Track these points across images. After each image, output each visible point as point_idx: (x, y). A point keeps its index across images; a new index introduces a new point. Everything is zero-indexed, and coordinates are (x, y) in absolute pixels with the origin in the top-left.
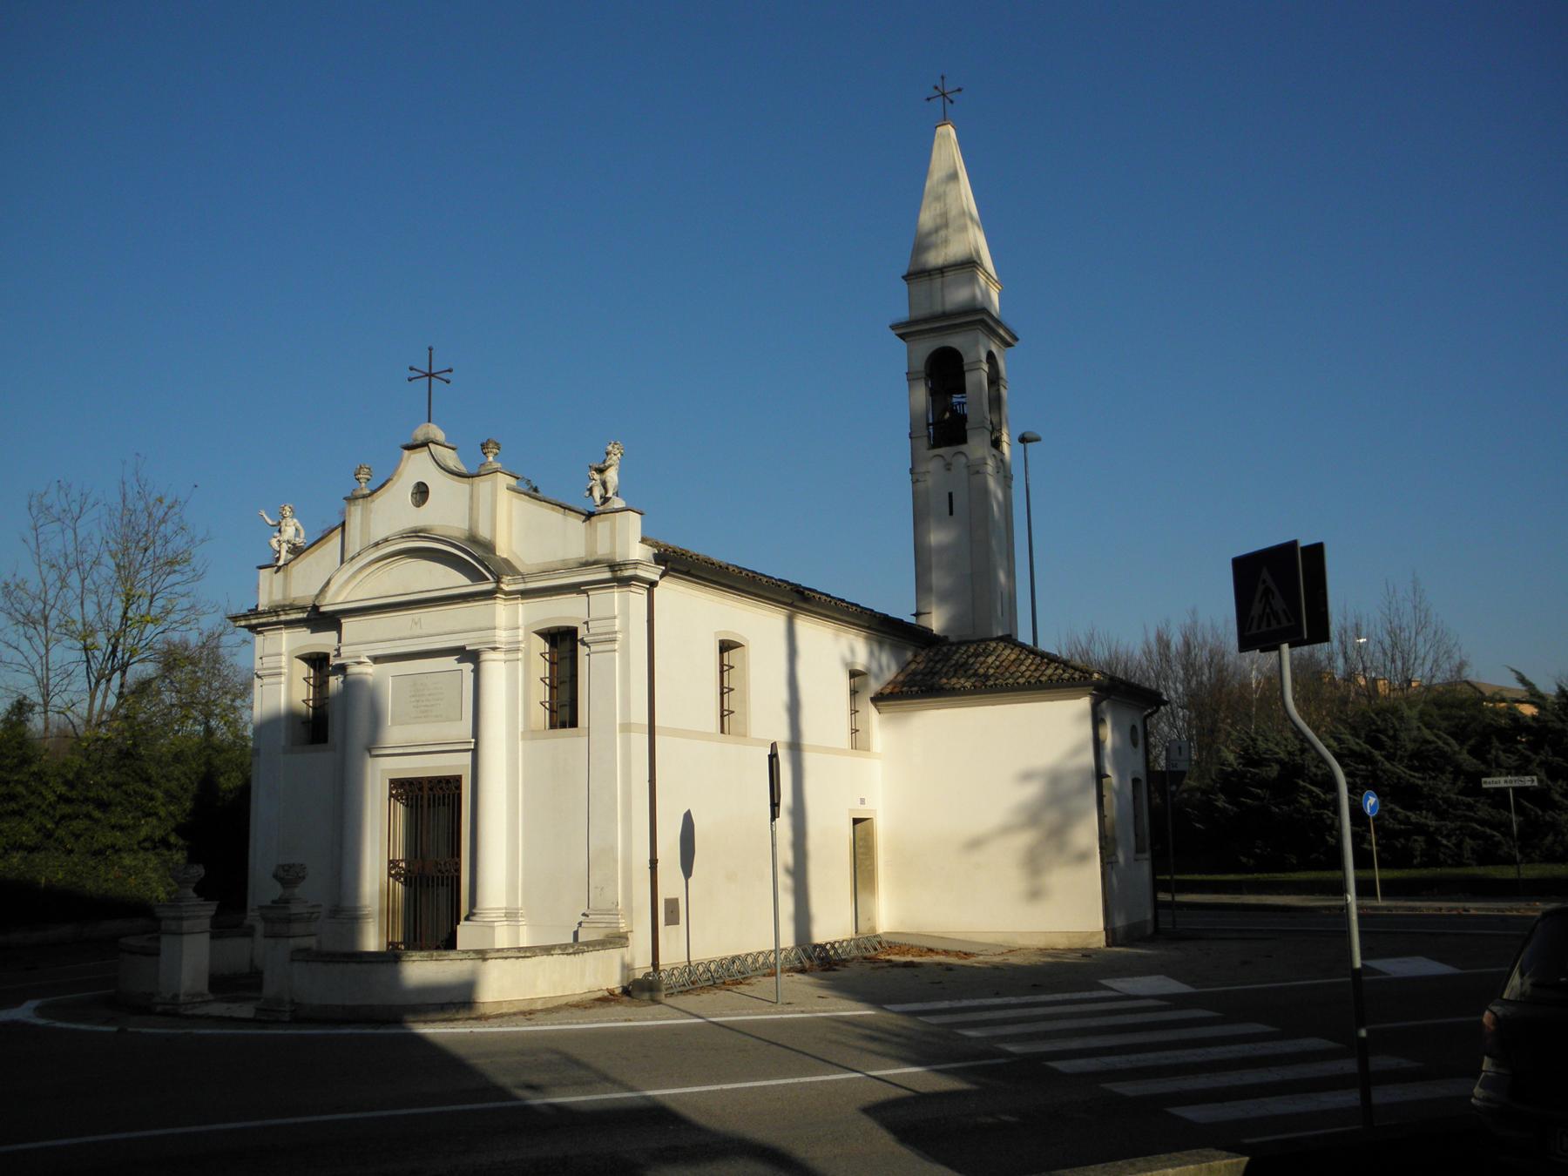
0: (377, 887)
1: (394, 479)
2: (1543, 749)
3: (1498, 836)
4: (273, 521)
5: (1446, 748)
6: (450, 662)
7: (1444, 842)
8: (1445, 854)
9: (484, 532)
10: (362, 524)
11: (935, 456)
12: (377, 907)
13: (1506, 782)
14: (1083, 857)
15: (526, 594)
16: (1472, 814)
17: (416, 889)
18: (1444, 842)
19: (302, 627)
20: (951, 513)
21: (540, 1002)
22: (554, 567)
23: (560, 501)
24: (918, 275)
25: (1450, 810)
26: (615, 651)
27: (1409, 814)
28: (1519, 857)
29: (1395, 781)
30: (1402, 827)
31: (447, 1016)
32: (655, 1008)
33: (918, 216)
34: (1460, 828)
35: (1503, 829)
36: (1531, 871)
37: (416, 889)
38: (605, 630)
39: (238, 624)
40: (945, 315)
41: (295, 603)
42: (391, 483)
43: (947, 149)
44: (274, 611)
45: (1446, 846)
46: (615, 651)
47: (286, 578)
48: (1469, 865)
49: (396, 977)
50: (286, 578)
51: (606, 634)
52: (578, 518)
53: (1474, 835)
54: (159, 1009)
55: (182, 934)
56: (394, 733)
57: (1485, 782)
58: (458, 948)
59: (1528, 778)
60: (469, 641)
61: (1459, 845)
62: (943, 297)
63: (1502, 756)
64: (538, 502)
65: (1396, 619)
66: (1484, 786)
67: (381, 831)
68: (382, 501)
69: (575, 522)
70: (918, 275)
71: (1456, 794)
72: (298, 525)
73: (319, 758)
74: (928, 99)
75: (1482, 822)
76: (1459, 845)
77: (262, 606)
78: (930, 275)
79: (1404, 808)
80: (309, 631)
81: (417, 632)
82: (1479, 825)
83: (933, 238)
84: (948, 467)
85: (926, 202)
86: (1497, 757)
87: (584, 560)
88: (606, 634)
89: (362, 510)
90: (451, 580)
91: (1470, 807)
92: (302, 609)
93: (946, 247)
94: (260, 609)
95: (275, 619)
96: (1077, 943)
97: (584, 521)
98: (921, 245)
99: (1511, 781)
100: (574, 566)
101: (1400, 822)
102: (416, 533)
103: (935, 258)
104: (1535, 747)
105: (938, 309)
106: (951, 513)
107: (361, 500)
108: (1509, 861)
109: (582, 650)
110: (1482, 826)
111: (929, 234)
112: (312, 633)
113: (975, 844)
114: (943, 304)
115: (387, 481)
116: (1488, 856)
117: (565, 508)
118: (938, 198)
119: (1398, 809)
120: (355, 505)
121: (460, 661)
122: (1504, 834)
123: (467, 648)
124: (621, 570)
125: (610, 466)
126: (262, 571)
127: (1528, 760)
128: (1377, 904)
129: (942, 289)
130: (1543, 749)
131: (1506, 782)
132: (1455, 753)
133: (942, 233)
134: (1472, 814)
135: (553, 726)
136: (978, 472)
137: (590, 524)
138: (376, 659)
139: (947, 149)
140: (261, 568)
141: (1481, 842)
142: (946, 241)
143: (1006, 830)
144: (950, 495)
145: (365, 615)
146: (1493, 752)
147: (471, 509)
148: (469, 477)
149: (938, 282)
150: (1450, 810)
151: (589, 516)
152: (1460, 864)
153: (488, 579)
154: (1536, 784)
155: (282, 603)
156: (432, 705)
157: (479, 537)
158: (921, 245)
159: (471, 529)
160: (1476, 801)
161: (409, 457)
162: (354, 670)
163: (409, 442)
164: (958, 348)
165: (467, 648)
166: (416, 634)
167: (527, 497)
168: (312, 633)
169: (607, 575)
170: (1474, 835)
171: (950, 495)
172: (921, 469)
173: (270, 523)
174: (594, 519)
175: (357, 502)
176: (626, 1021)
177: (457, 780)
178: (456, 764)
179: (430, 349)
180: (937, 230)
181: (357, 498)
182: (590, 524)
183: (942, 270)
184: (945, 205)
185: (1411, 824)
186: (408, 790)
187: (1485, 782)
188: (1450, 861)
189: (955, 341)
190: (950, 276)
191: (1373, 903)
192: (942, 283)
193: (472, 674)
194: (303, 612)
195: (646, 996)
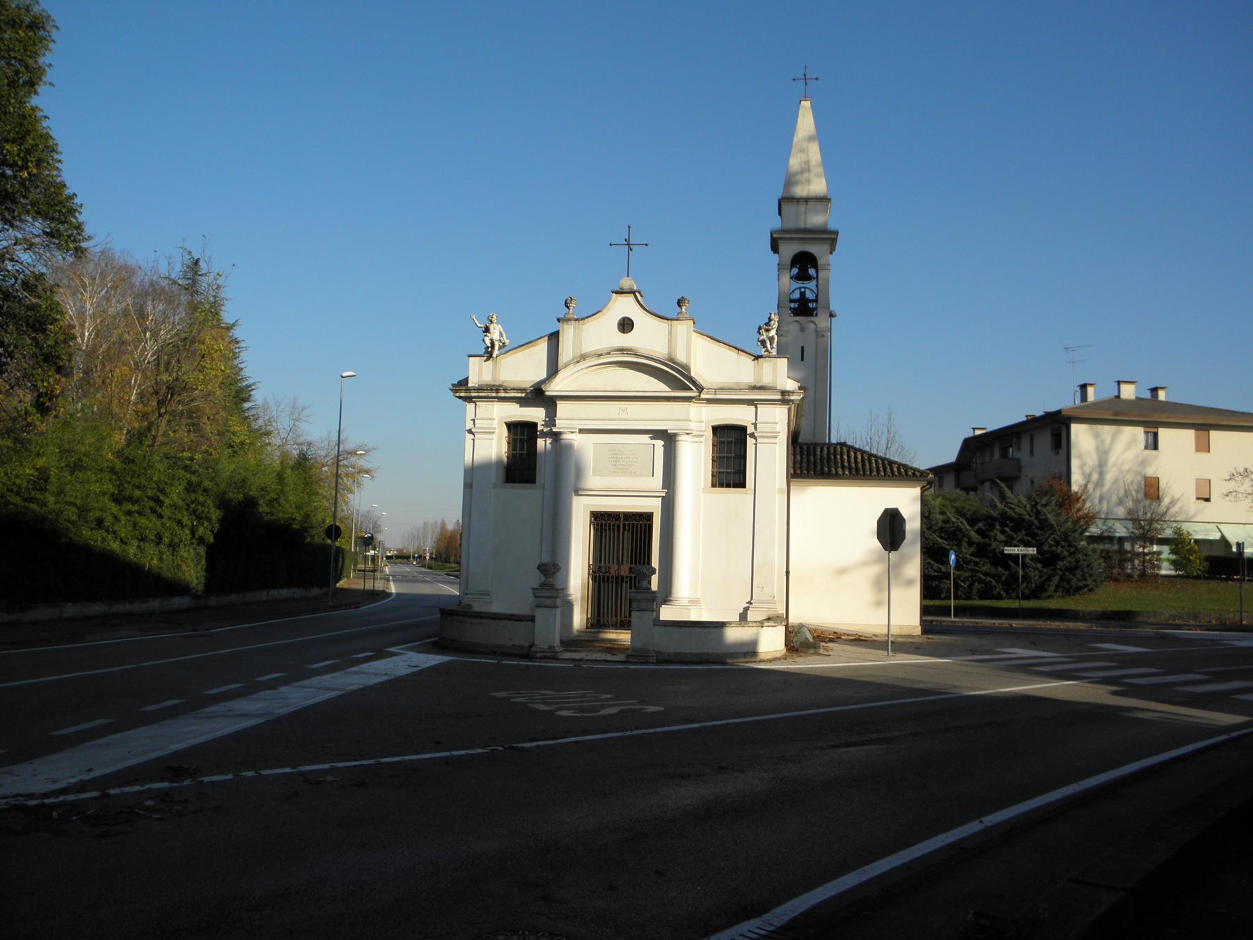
0: (580, 583)
1: (603, 311)
2: (1021, 532)
3: (994, 583)
4: (480, 324)
5: (963, 527)
6: (646, 439)
7: (963, 584)
8: (961, 591)
9: (681, 357)
10: (574, 337)
11: (796, 321)
12: (579, 595)
13: (1018, 550)
14: (910, 583)
15: (709, 401)
16: (977, 568)
17: (599, 583)
18: (963, 584)
19: (513, 402)
20: (802, 359)
21: (778, 653)
22: (730, 386)
23: (735, 345)
24: (786, 201)
25: (965, 565)
26: (776, 443)
27: (941, 566)
28: (1004, 595)
29: (931, 545)
30: (936, 574)
31: (747, 660)
32: (817, 658)
33: (788, 160)
34: (971, 577)
35: (996, 578)
36: (1014, 604)
37: (599, 583)
38: (769, 430)
39: (457, 395)
40: (806, 231)
41: (504, 384)
42: (600, 313)
43: (806, 122)
44: (479, 389)
45: (963, 588)
46: (776, 443)
47: (495, 366)
48: (974, 599)
49: (721, 636)
50: (495, 366)
51: (771, 432)
52: (750, 358)
53: (980, 581)
54: (539, 655)
55: (556, 607)
56: (592, 481)
57: (1006, 550)
58: (748, 620)
59: (1031, 549)
60: (670, 427)
61: (970, 586)
62: (806, 218)
63: (999, 534)
64: (717, 343)
65: (876, 436)
66: (1006, 552)
67: (583, 545)
68: (591, 325)
69: (747, 361)
70: (786, 201)
71: (971, 555)
72: (501, 329)
73: (520, 493)
74: (794, 80)
75: (986, 574)
76: (970, 586)
77: (472, 383)
78: (798, 202)
79: (936, 562)
80: (518, 405)
81: (624, 417)
82: (983, 575)
83: (799, 177)
84: (802, 329)
85: (793, 151)
86: (996, 535)
87: (753, 385)
88: (771, 432)
89: (575, 328)
90: (657, 387)
91: (976, 564)
92: (522, 390)
93: (809, 185)
94: (470, 385)
95: (494, 395)
96: (905, 632)
97: (754, 360)
98: (790, 181)
99: (1021, 551)
100: (746, 388)
101: (935, 571)
102: (622, 350)
103: (800, 191)
104: (1015, 530)
105: (802, 225)
106: (802, 359)
107: (573, 322)
108: (999, 597)
109: (750, 441)
110: (986, 576)
111: (796, 174)
112: (520, 407)
113: (842, 571)
114: (806, 222)
115: (598, 312)
116: (984, 595)
117: (738, 350)
118: (802, 150)
119: (933, 563)
120: (567, 324)
121: (652, 438)
122: (997, 582)
123: (669, 432)
124: (789, 395)
125: (773, 329)
126: (471, 358)
127: (1013, 539)
128: (950, 619)
129: (806, 213)
130: (1021, 532)
131: (1018, 550)
132: (967, 530)
133: (806, 175)
134: (977, 568)
135: (713, 485)
136: (823, 336)
137: (758, 363)
138: (581, 431)
139: (806, 122)
140: (470, 356)
141: (983, 585)
142: (809, 181)
143: (864, 564)
144: (803, 348)
145: (578, 401)
146: (995, 531)
147: (670, 341)
148: (668, 320)
149: (802, 207)
150: (965, 565)
151: (757, 358)
152: (969, 598)
153: (692, 390)
154: (1035, 552)
155: (492, 383)
156: (629, 465)
157: (676, 360)
158: (790, 181)
159: (669, 354)
160: (981, 561)
161: (617, 299)
162: (567, 437)
163: (617, 289)
164: (816, 255)
165: (669, 432)
166: (624, 417)
167: (708, 339)
168: (520, 407)
169: (779, 397)
170: (980, 581)
171: (803, 348)
172: (785, 328)
173: (479, 325)
174: (760, 360)
175: (570, 322)
176: (846, 662)
177: (648, 517)
178: (654, 506)
179: (629, 227)
180: (802, 172)
181: (569, 320)
182: (758, 363)
183: (806, 200)
184: (808, 156)
185: (941, 572)
186: (603, 522)
187: (1006, 550)
188: (963, 596)
189: (812, 249)
190: (811, 205)
191: (950, 619)
192: (806, 209)
193: (663, 448)
194: (522, 393)
195: (812, 651)
